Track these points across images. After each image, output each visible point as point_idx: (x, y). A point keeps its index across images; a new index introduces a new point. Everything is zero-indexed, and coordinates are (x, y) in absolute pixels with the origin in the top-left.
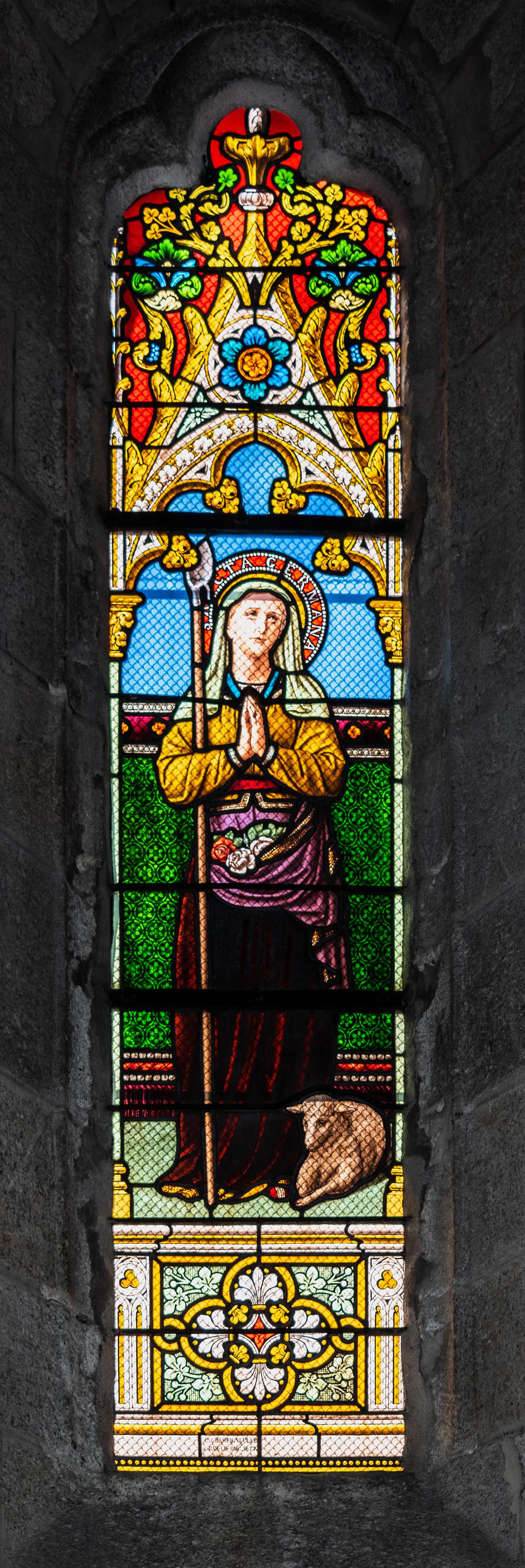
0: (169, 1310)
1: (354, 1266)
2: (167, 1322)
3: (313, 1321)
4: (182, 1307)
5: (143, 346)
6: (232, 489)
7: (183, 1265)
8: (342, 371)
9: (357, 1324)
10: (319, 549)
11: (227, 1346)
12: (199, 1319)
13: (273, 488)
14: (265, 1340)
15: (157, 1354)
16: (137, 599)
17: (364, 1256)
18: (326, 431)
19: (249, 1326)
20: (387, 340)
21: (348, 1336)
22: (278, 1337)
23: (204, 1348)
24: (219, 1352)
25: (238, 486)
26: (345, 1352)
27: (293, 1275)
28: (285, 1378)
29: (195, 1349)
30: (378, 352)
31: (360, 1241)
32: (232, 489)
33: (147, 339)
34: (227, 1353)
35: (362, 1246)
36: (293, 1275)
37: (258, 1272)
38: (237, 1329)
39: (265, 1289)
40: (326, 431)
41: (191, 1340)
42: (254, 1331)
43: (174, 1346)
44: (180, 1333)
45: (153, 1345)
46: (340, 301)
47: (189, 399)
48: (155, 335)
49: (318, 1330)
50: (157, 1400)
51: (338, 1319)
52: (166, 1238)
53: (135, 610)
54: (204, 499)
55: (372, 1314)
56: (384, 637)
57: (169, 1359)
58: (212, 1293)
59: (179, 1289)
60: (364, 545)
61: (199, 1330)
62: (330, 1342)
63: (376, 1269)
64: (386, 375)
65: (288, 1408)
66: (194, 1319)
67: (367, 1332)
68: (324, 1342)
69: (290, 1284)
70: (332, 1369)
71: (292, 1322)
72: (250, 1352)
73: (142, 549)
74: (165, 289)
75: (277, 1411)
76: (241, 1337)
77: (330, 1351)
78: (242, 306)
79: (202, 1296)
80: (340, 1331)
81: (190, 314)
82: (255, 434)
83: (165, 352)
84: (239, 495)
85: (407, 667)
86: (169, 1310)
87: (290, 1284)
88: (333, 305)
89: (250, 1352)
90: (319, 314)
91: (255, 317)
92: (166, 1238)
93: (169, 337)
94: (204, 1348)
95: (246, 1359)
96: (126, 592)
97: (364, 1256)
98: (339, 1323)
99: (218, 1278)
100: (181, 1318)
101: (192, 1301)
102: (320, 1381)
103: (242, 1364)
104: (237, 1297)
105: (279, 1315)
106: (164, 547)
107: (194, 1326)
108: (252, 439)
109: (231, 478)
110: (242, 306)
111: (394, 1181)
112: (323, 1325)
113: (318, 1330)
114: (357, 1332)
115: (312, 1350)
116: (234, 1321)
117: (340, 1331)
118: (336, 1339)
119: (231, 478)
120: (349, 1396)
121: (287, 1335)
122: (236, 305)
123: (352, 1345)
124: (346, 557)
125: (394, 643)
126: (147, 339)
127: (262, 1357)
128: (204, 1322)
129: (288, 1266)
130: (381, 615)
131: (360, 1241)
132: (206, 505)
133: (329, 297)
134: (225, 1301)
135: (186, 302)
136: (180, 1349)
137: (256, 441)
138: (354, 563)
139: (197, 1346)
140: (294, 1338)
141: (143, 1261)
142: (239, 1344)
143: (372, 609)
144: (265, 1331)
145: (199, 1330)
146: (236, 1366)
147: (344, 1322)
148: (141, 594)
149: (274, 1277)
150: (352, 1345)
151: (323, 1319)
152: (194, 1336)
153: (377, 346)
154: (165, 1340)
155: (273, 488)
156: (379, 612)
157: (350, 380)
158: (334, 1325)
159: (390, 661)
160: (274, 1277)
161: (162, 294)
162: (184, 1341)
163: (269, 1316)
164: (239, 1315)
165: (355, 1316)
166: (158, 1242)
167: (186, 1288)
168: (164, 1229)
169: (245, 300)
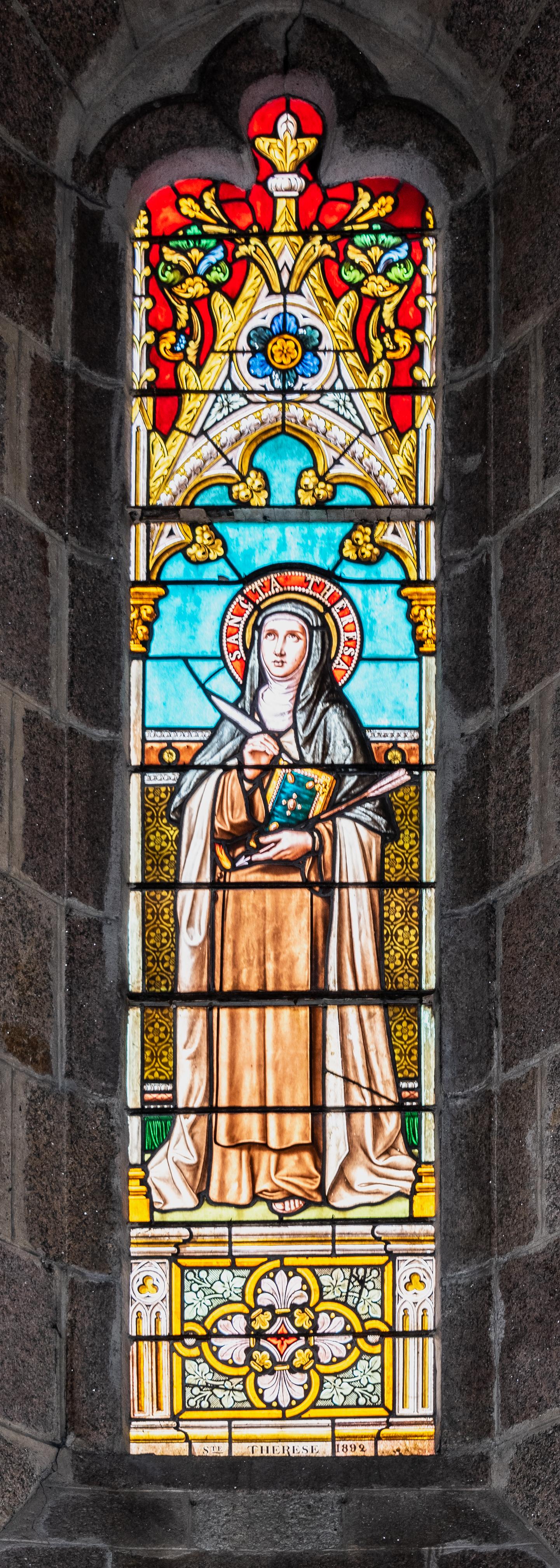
0: (189, 1314)
1: (381, 1268)
2: (188, 1327)
3: (338, 1325)
4: (203, 1312)
5: (171, 336)
6: (258, 482)
7: (207, 1268)
8: (375, 360)
9: (384, 1328)
10: (348, 536)
11: (249, 1351)
12: (221, 1323)
13: (300, 477)
14: (288, 1345)
15: (177, 1360)
16: (160, 590)
17: (392, 1256)
18: (357, 421)
19: (272, 1331)
20: (424, 294)
21: (372, 1339)
22: (302, 1342)
23: (224, 1354)
24: (241, 1358)
25: (265, 477)
26: (372, 1355)
27: (317, 1277)
28: (309, 1382)
29: (215, 1354)
30: (413, 339)
31: (387, 1242)
32: (258, 482)
33: (173, 327)
34: (249, 1358)
35: (389, 1247)
36: (317, 1277)
37: (281, 1275)
38: (260, 1335)
39: (289, 1292)
40: (357, 421)
41: (211, 1346)
42: (277, 1336)
43: (195, 1352)
44: (200, 1339)
45: (172, 1350)
46: (374, 286)
47: (218, 387)
48: (182, 323)
49: (344, 1333)
50: (178, 1407)
51: (363, 1322)
52: (185, 1242)
53: (157, 600)
54: (230, 493)
55: (400, 1314)
56: (415, 624)
57: (190, 1365)
58: (331, 1379)
59: (201, 1294)
60: (395, 532)
61: (220, 1335)
62: (354, 1344)
63: (405, 1268)
64: (420, 363)
65: (313, 1413)
66: (215, 1325)
67: (393, 1333)
68: (349, 1346)
69: (314, 1286)
70: (356, 1373)
71: (315, 1327)
72: (272, 1358)
73: (165, 543)
74: (192, 277)
75: (298, 1417)
76: (263, 1343)
77: (356, 1353)
78: (271, 292)
79: (223, 1301)
80: (364, 1334)
81: (218, 300)
82: (283, 425)
83: (191, 343)
84: (267, 487)
85: (439, 654)
86: (189, 1314)
87: (314, 1286)
88: (364, 290)
89: (272, 1358)
90: (350, 299)
91: (285, 304)
92: (185, 1242)
93: (197, 327)
94: (224, 1354)
95: (268, 1364)
96: (148, 583)
97: (392, 1256)
98: (363, 1326)
99: (239, 1282)
100: (202, 1323)
101: (215, 1305)
102: (345, 1385)
103: (265, 1372)
104: (259, 1303)
105: (303, 1320)
106: (189, 540)
107: (215, 1331)
108: (279, 430)
109: (258, 470)
110: (271, 292)
111: (421, 1181)
112: (348, 1328)
113: (344, 1333)
114: (383, 1335)
115: (337, 1354)
116: (256, 1326)
117: (364, 1334)
118: (361, 1342)
119: (258, 470)
120: (375, 1399)
121: (311, 1339)
122: (266, 290)
123: (379, 1346)
124: (376, 545)
125: (428, 630)
126: (173, 327)
127: (283, 1364)
128: (224, 1327)
129: (312, 1268)
130: (414, 603)
131: (387, 1242)
132: (231, 498)
133: (360, 284)
134: (248, 1306)
135: (214, 287)
136: (202, 1355)
137: (283, 432)
138: (384, 549)
139: (217, 1352)
140: (319, 1341)
141: (163, 1266)
142: (261, 1349)
143: (405, 598)
144: (288, 1336)
145: (220, 1335)
146: (247, 1317)
147: (369, 1325)
148: (164, 584)
149: (298, 1279)
150: (379, 1346)
151: (347, 1322)
152: (213, 1340)
153: (412, 333)
154: (185, 1345)
155: (300, 477)
156: (411, 600)
157: (383, 369)
158: (358, 1329)
159: (421, 649)
160: (298, 1279)
161: (189, 281)
162: (205, 1345)
163: (292, 1319)
164: (262, 1321)
165: (382, 1319)
166: (177, 1245)
167: (208, 1292)
168: (184, 1232)
169: (273, 288)
